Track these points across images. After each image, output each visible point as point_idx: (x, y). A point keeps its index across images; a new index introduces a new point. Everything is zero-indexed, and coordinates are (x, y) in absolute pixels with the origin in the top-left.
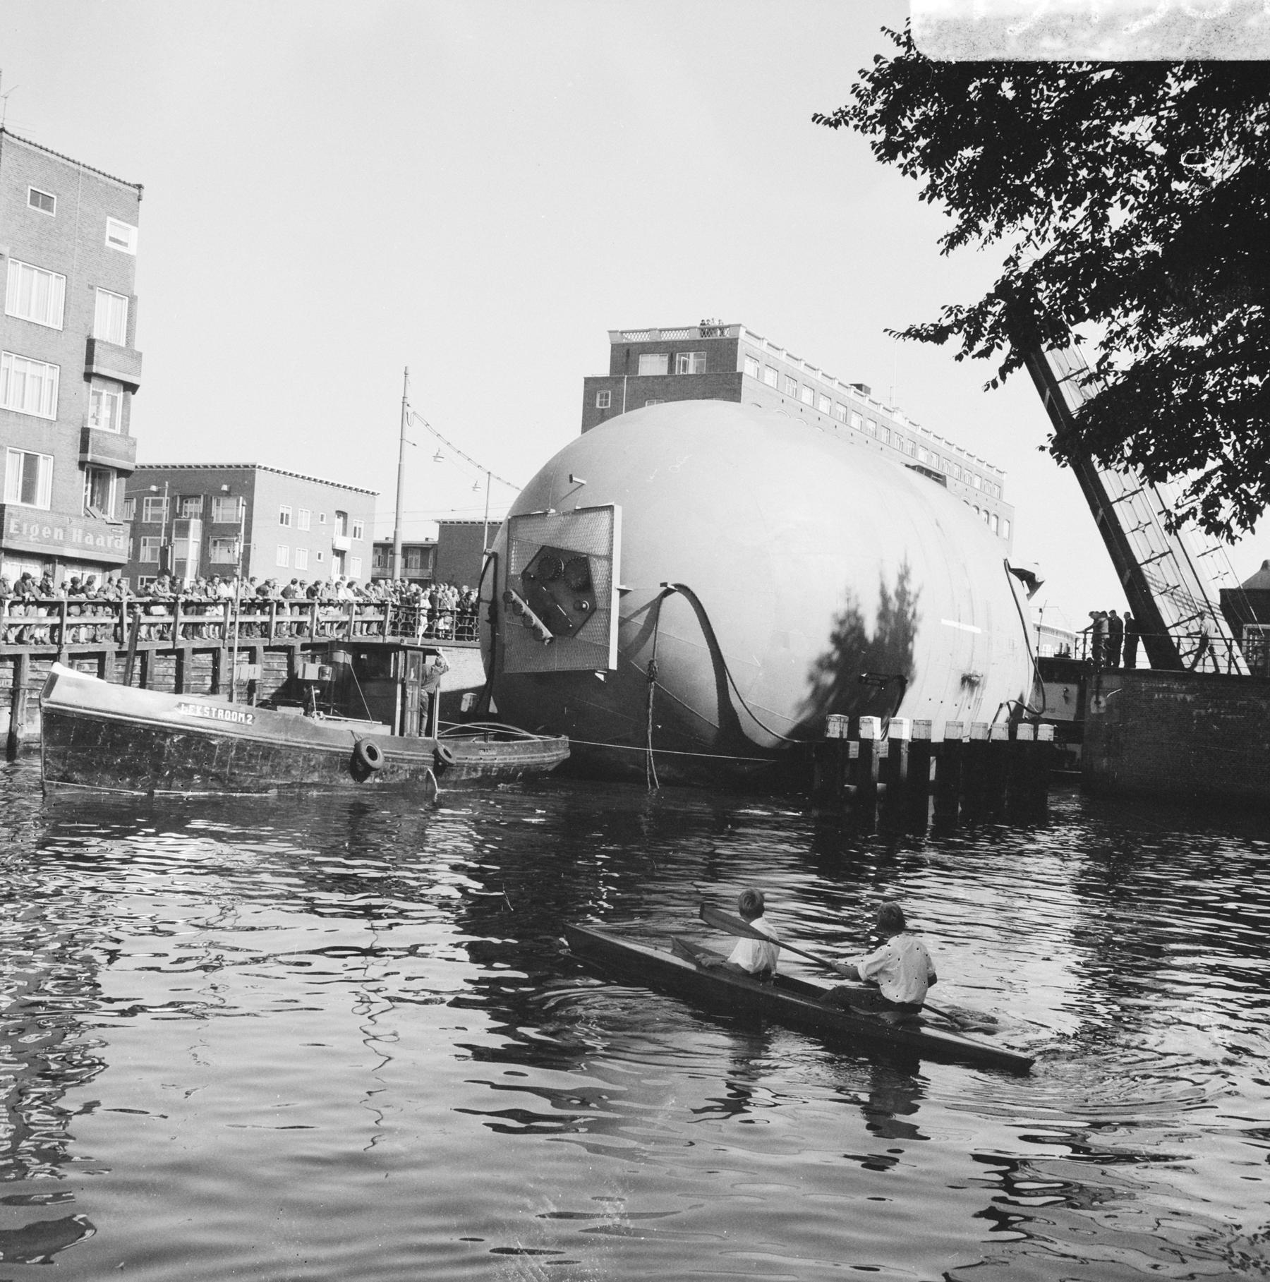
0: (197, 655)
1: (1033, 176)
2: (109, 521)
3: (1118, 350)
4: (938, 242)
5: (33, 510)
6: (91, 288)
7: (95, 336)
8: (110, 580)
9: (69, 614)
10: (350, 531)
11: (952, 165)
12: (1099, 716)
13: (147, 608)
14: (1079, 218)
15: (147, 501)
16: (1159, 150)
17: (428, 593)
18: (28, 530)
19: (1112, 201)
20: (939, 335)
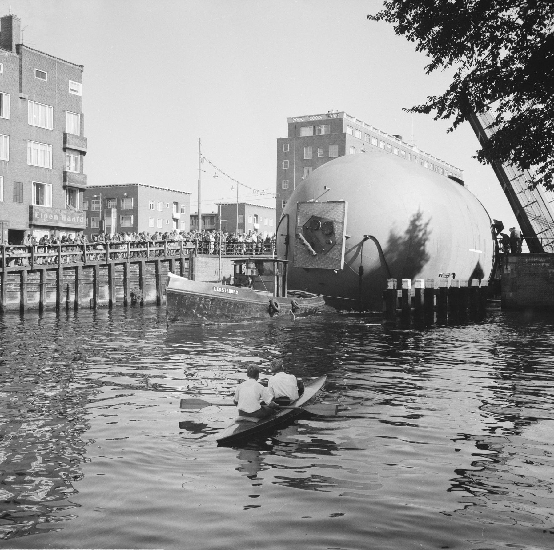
0: (117, 266)
1: (465, 37)
2: (77, 211)
3: (505, 111)
4: (424, 69)
5: (44, 208)
6: (64, 111)
7: (67, 132)
8: (79, 235)
9: (62, 251)
10: (180, 210)
11: (429, 34)
12: (508, 274)
13: (95, 247)
14: (486, 55)
15: (93, 202)
16: (520, 22)
17: (213, 234)
18: (43, 216)
19: (501, 46)
20: (427, 109)
